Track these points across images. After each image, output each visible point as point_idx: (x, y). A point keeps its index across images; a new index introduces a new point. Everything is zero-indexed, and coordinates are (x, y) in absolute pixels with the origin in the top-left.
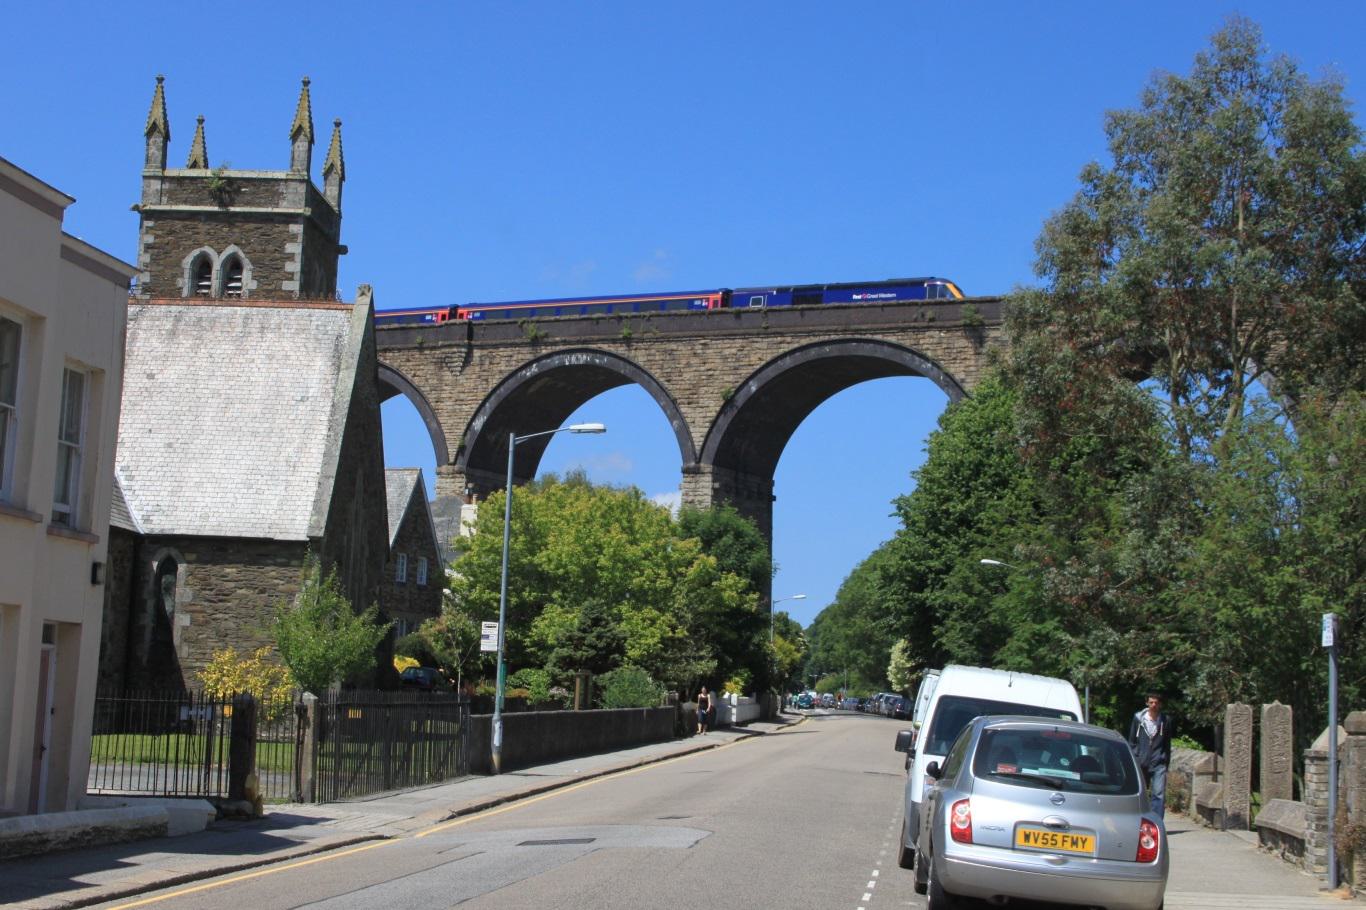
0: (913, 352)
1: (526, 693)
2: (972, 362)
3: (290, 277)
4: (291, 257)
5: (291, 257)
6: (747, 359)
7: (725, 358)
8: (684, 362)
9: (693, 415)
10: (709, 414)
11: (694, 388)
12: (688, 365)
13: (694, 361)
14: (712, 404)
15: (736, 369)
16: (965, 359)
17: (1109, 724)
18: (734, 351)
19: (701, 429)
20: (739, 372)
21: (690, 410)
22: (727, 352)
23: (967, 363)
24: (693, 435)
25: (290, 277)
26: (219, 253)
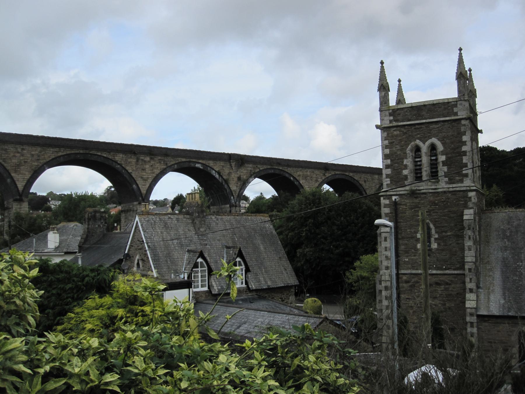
0: (113, 161)
1: (54, 357)
2: (134, 167)
3: (386, 206)
4: (406, 167)
5: (406, 167)
6: (43, 157)
7: (33, 155)
8: (12, 155)
9: (18, 177)
10: (25, 177)
11: (19, 165)
12: (15, 156)
13: (18, 155)
14: (27, 173)
15: (38, 160)
16: (132, 165)
17: (341, 348)
18: (37, 152)
19: (22, 183)
20: (39, 161)
21: (16, 175)
22: (33, 153)
23: (133, 167)
24: (18, 185)
25: (386, 206)
26: (424, 143)
